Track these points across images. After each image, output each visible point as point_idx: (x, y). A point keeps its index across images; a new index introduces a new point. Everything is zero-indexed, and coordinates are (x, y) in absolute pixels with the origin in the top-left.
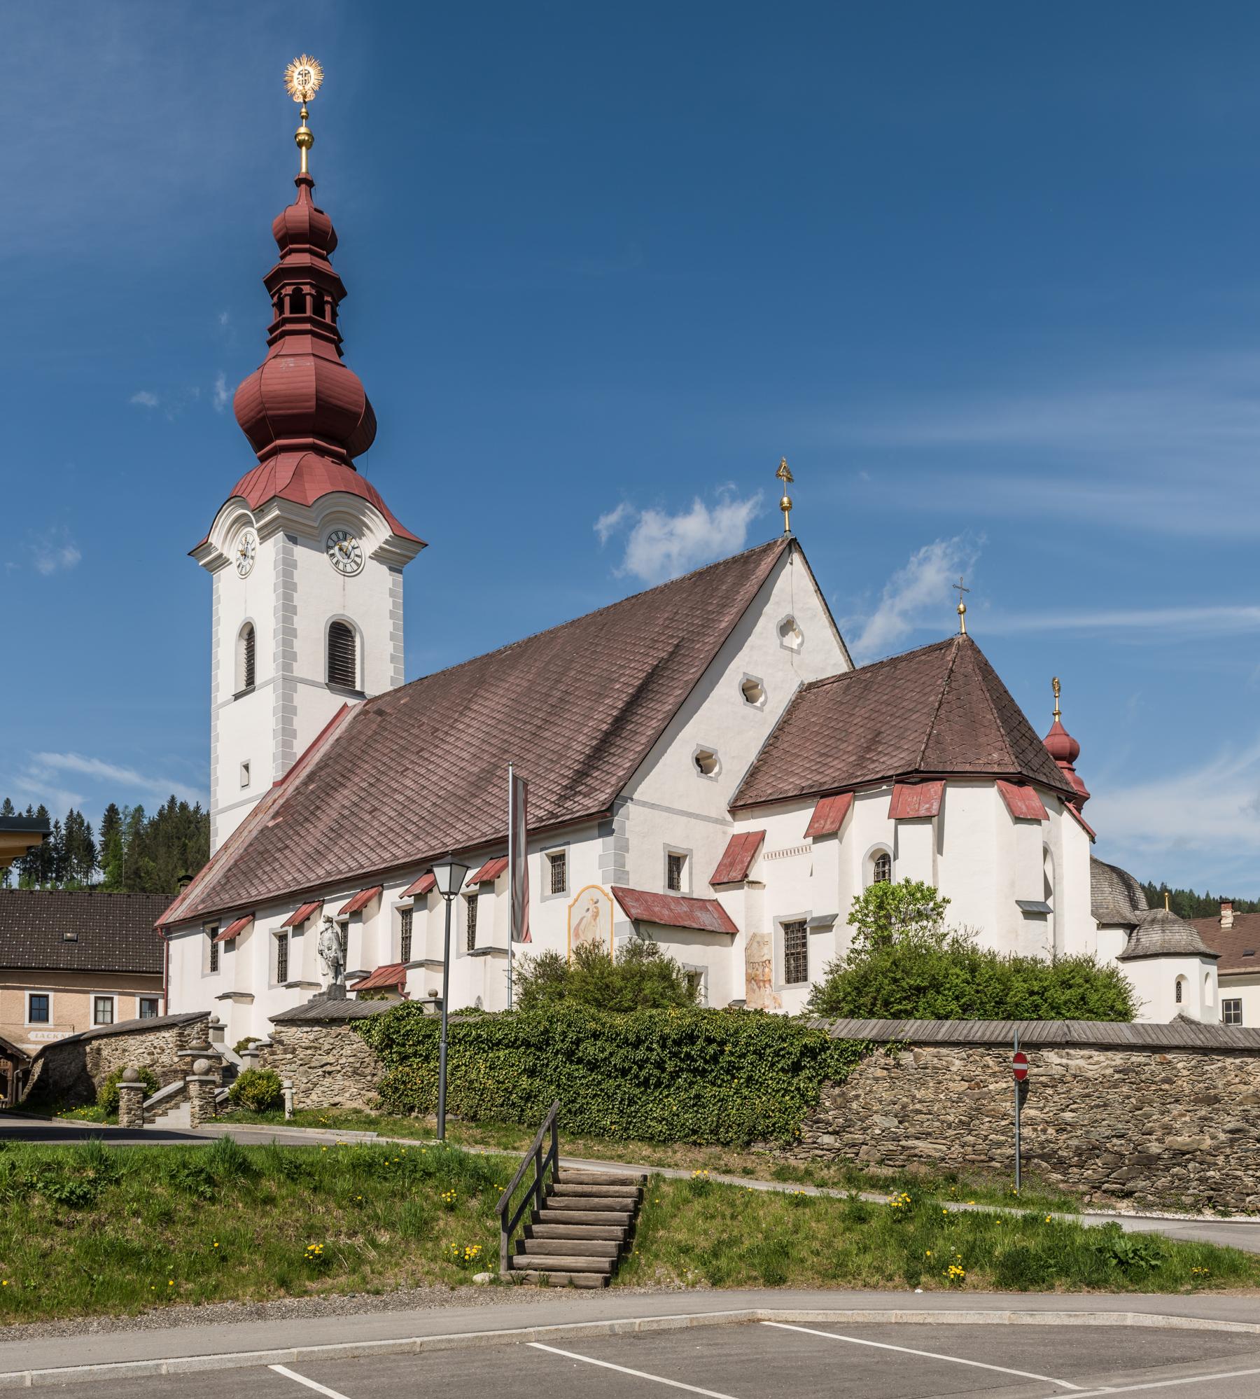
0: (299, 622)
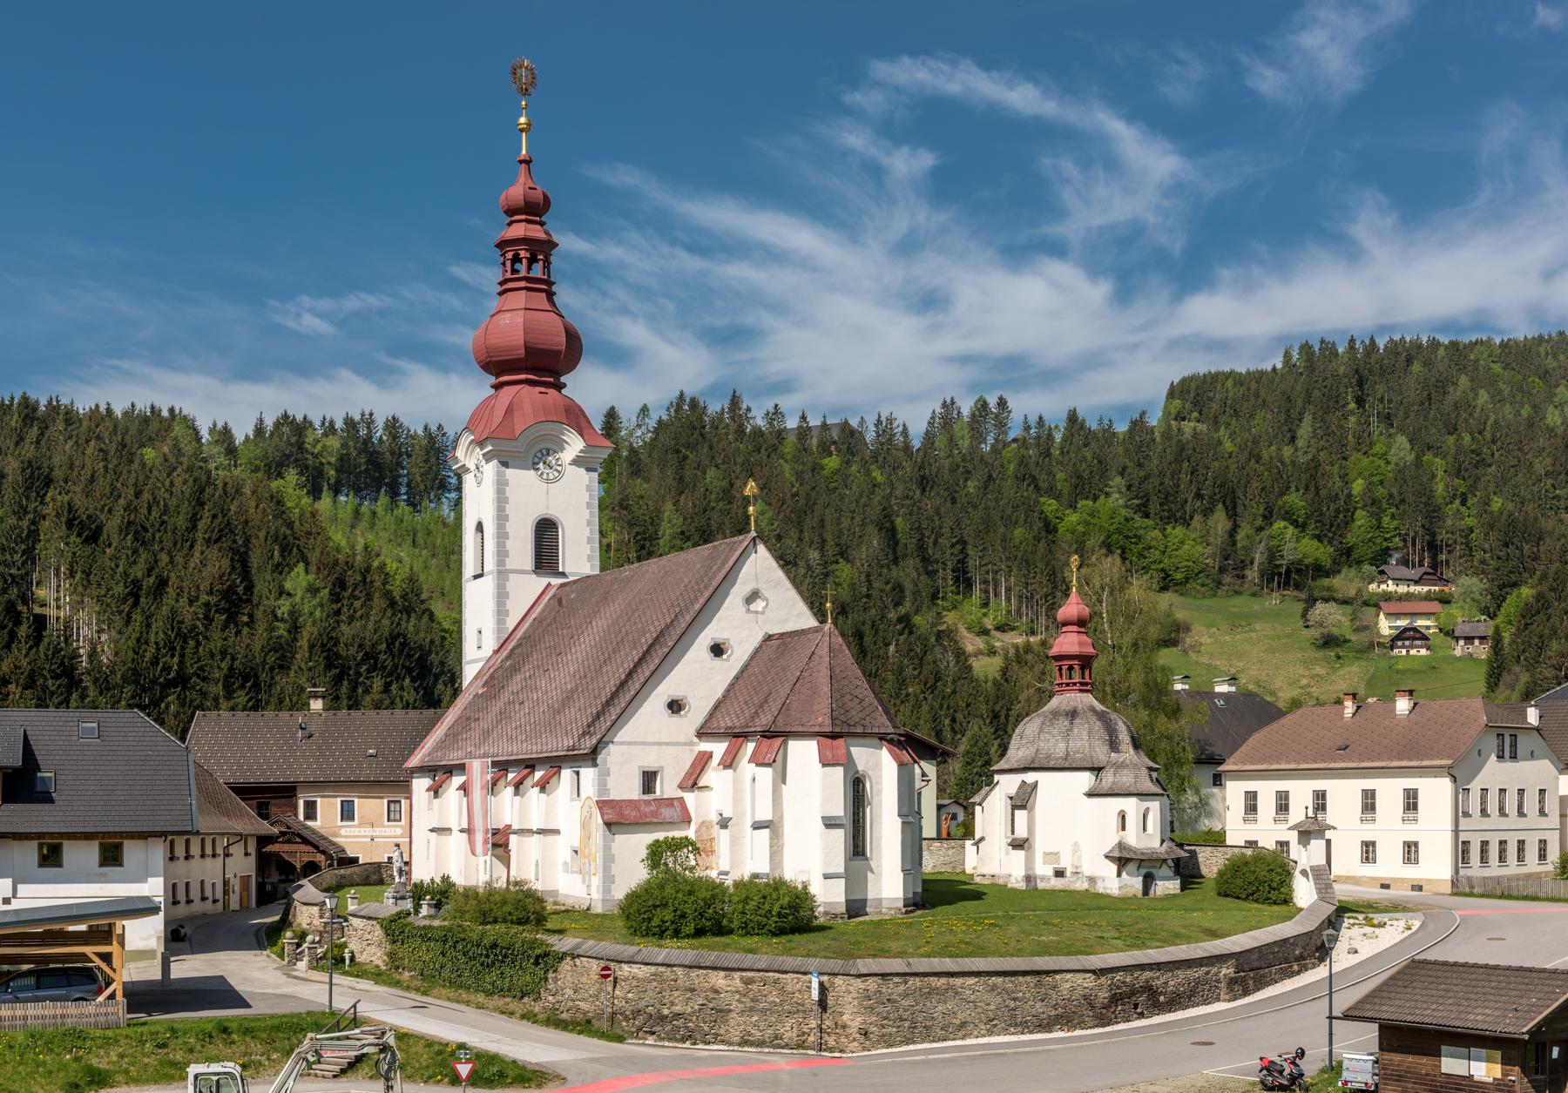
0: (510, 527)
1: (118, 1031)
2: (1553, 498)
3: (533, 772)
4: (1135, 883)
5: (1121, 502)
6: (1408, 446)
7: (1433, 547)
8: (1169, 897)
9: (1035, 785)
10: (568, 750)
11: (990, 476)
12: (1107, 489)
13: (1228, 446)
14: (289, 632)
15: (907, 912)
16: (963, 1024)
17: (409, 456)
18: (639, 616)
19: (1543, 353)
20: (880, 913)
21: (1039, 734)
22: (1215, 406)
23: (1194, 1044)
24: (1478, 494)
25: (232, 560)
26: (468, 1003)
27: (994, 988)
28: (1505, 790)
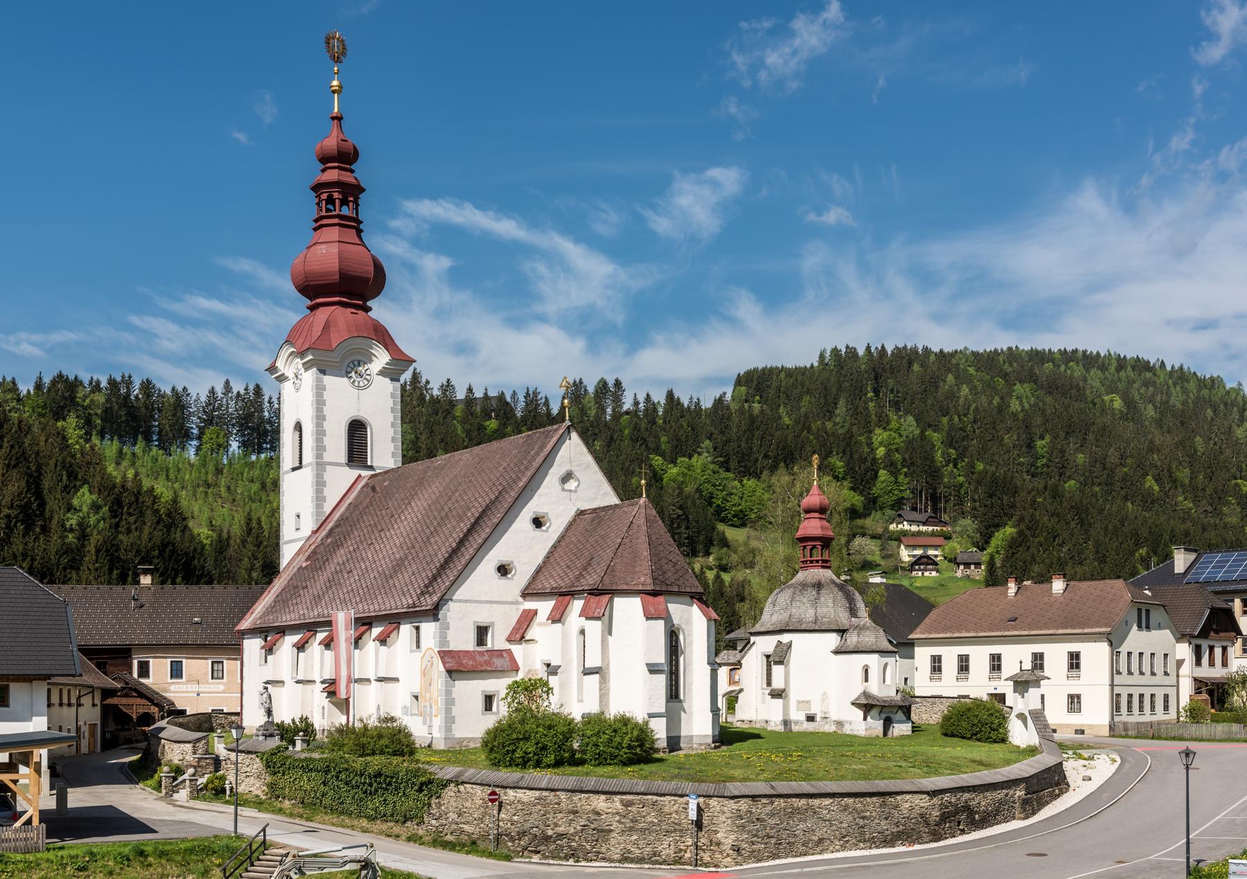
0: (327, 426)
1: (38, 855)
2: (1019, 464)
3: (370, 629)
4: (877, 726)
5: (709, 459)
6: (915, 423)
7: (935, 499)
8: (903, 737)
9: (790, 645)
10: (409, 608)
11: (612, 438)
12: (699, 450)
13: (787, 420)
14: (79, 539)
15: (716, 748)
16: (821, 841)
17: (160, 410)
18: (460, 495)
19: (1002, 362)
20: (692, 748)
21: (791, 602)
22: (772, 392)
23: (1029, 855)
24: (966, 460)
25: (27, 482)
26: (352, 827)
27: (846, 808)
28: (1143, 653)
